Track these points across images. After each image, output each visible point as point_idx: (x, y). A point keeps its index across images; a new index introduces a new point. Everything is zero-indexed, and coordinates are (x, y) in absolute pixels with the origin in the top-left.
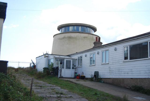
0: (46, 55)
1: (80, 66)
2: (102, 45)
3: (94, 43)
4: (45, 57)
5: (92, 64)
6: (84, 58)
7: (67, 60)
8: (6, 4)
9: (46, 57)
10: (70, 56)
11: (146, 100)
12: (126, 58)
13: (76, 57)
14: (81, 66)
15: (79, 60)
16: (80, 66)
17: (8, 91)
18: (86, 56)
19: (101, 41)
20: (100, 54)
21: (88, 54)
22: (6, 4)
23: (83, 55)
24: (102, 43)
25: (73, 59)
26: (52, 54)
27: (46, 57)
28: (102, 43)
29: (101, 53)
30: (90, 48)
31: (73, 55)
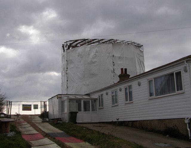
0: (59, 96)
1: (101, 107)
2: (130, 77)
3: (120, 76)
4: (57, 98)
5: (114, 104)
6: (105, 97)
7: (85, 100)
8: (23, 110)
9: (58, 98)
10: (89, 95)
11: (168, 146)
12: (151, 95)
13: (95, 96)
14: (130, 102)
15: (99, 99)
16: (101, 107)
17: (67, 46)
18: (107, 94)
19: (128, 73)
20: (122, 90)
21: (109, 91)
22: (23, 110)
23: (104, 93)
24: (129, 76)
25: (92, 99)
26: (67, 94)
27: (58, 98)
28: (129, 76)
29: (123, 90)
30: (134, 76)
31: (92, 94)
